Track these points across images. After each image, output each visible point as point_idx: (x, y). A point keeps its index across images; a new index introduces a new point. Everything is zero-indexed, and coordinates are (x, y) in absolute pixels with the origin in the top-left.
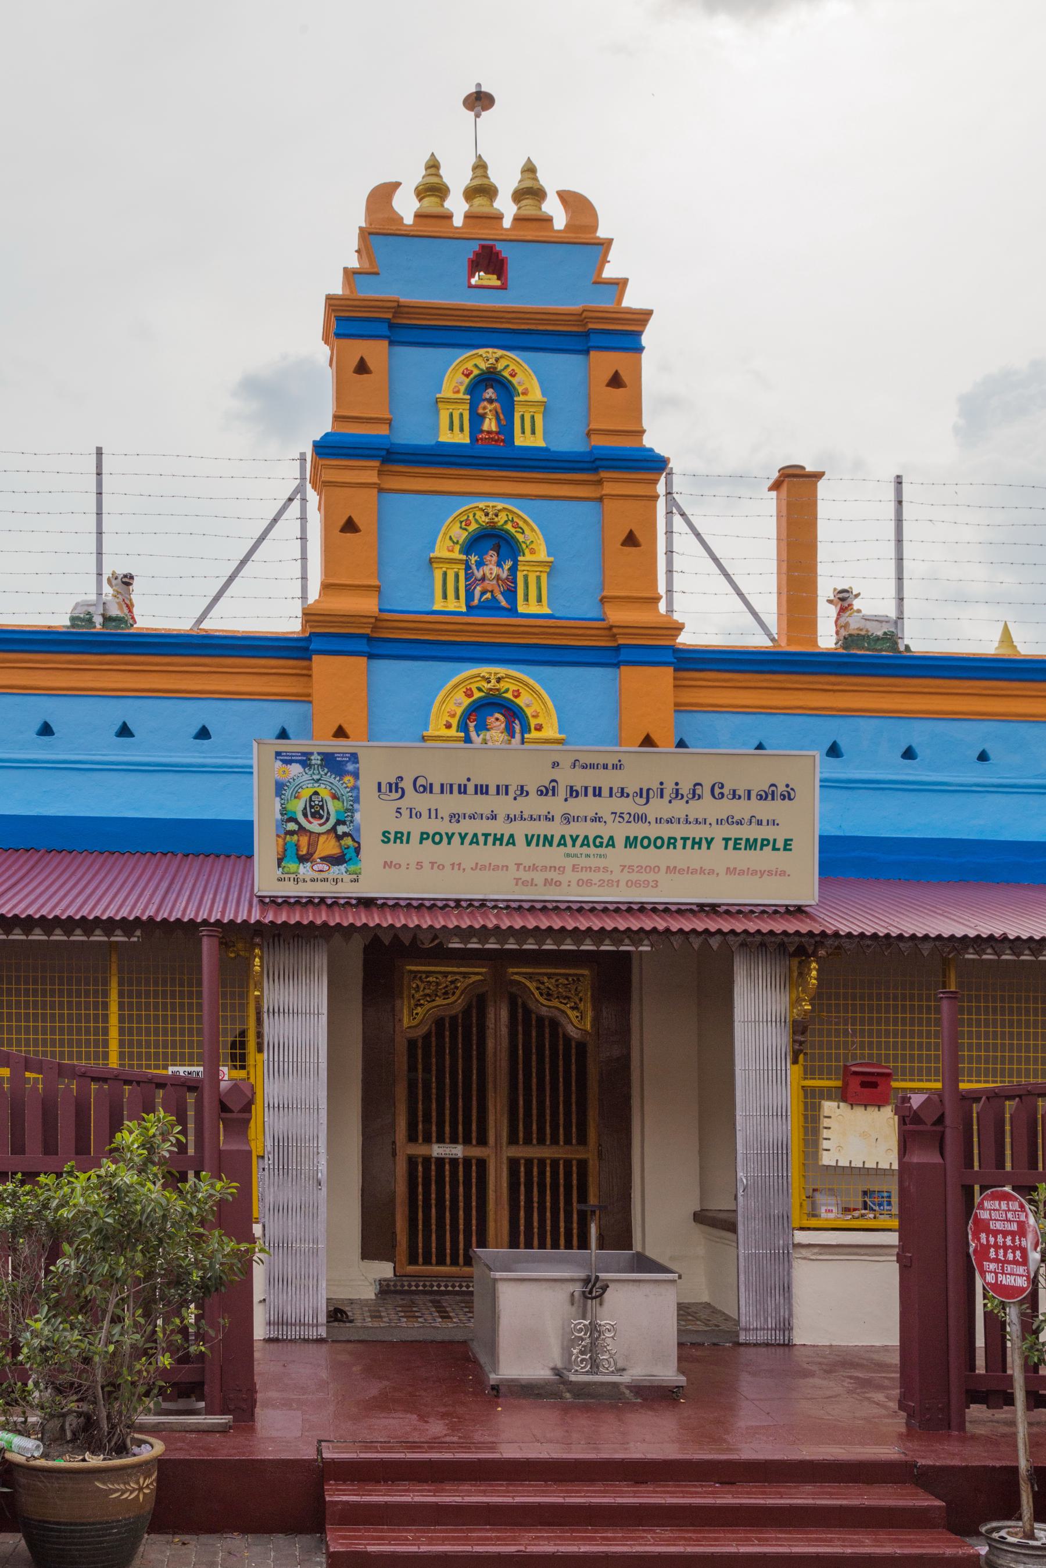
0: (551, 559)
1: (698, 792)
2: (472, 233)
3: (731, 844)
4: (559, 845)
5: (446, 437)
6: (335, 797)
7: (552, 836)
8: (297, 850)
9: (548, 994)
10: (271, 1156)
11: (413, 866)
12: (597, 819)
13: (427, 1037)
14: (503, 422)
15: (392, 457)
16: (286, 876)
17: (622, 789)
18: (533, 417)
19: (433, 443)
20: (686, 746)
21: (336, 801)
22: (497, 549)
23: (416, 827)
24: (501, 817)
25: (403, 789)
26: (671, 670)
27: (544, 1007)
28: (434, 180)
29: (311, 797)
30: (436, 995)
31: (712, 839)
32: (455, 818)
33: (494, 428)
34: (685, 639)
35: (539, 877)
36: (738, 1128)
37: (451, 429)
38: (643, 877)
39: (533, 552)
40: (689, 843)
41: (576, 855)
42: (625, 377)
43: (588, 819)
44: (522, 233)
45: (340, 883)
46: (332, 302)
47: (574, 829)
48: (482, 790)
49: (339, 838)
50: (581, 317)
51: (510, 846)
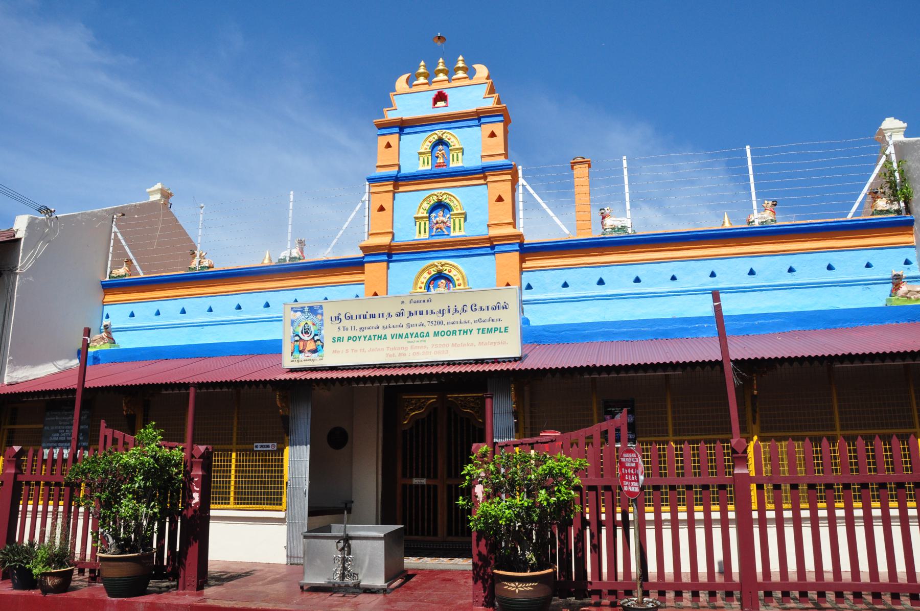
12: (421, 325)
32: (362, 329)
48: (373, 316)
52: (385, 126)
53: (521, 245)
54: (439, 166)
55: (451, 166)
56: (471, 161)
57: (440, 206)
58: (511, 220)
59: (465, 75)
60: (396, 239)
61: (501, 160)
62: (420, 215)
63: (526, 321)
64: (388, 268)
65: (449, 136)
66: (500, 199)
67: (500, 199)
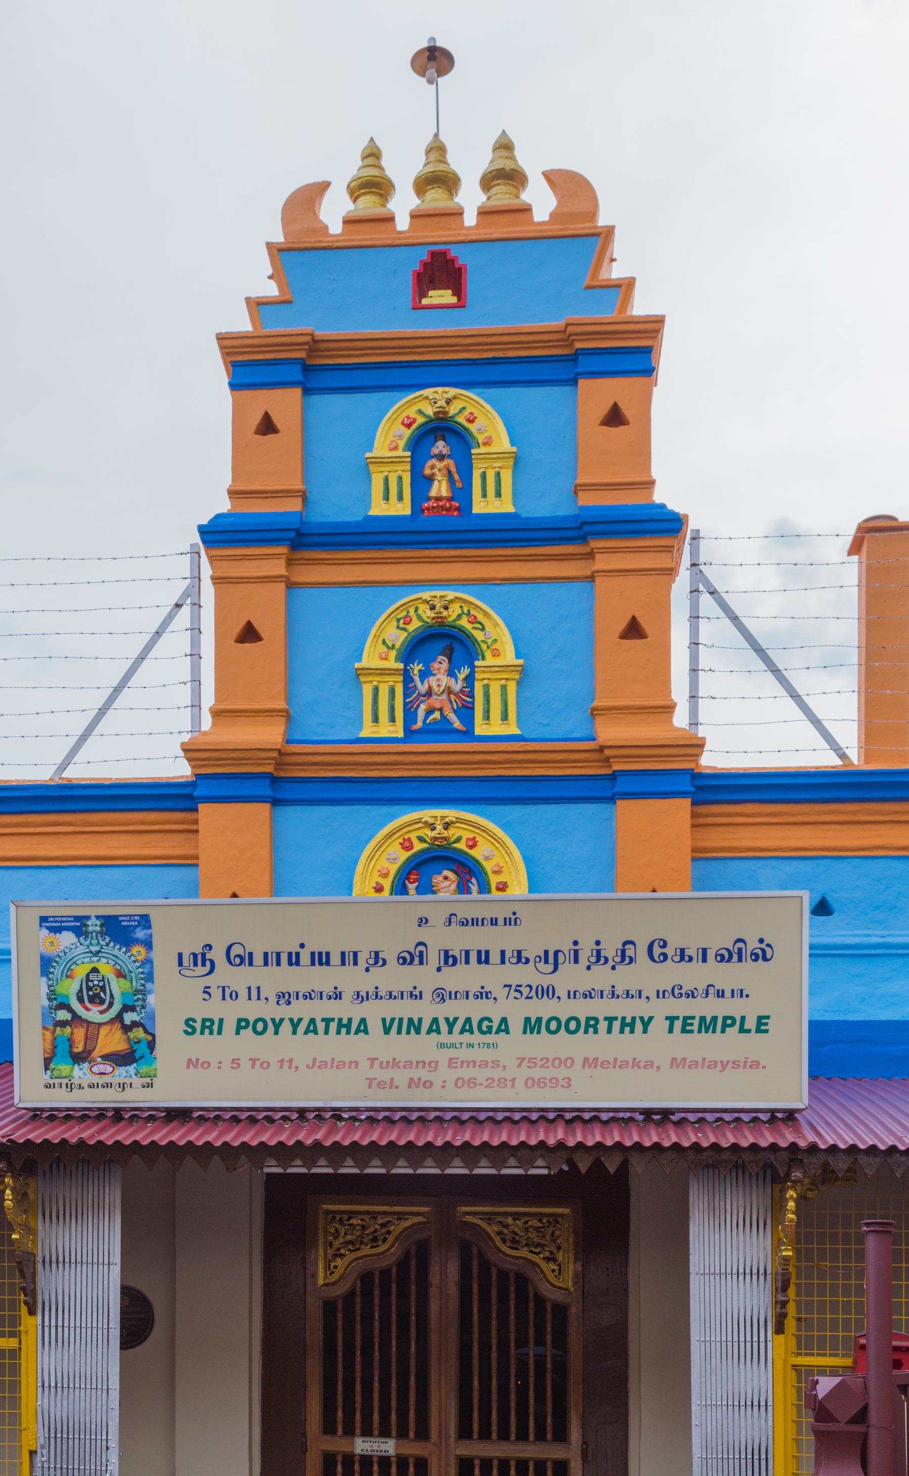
0: (521, 662)
1: (630, 952)
3: (678, 1024)
4: (429, 1032)
5: (379, 509)
6: (120, 974)
7: (420, 1020)
8: (71, 1047)
9: (514, 1241)
10: (44, 1452)
11: (227, 1064)
12: (483, 995)
13: (350, 1297)
14: (459, 485)
15: (303, 540)
16: (57, 1081)
17: (519, 952)
18: (498, 475)
19: (359, 518)
21: (121, 980)
22: (449, 653)
23: (230, 1012)
24: (348, 996)
25: (212, 962)
26: (687, 802)
27: (508, 1255)
28: (374, 172)
29: (88, 976)
30: (362, 1243)
32: (284, 998)
33: (445, 492)
34: (712, 760)
35: (401, 1077)
36: (694, 1422)
37: (386, 498)
38: (549, 1073)
39: (496, 654)
40: (616, 1025)
41: (453, 1046)
42: (627, 410)
43: (471, 995)
44: (488, 231)
45: (128, 1089)
46: (225, 343)
47: (451, 1009)
48: (321, 959)
49: (126, 1029)
50: (565, 335)
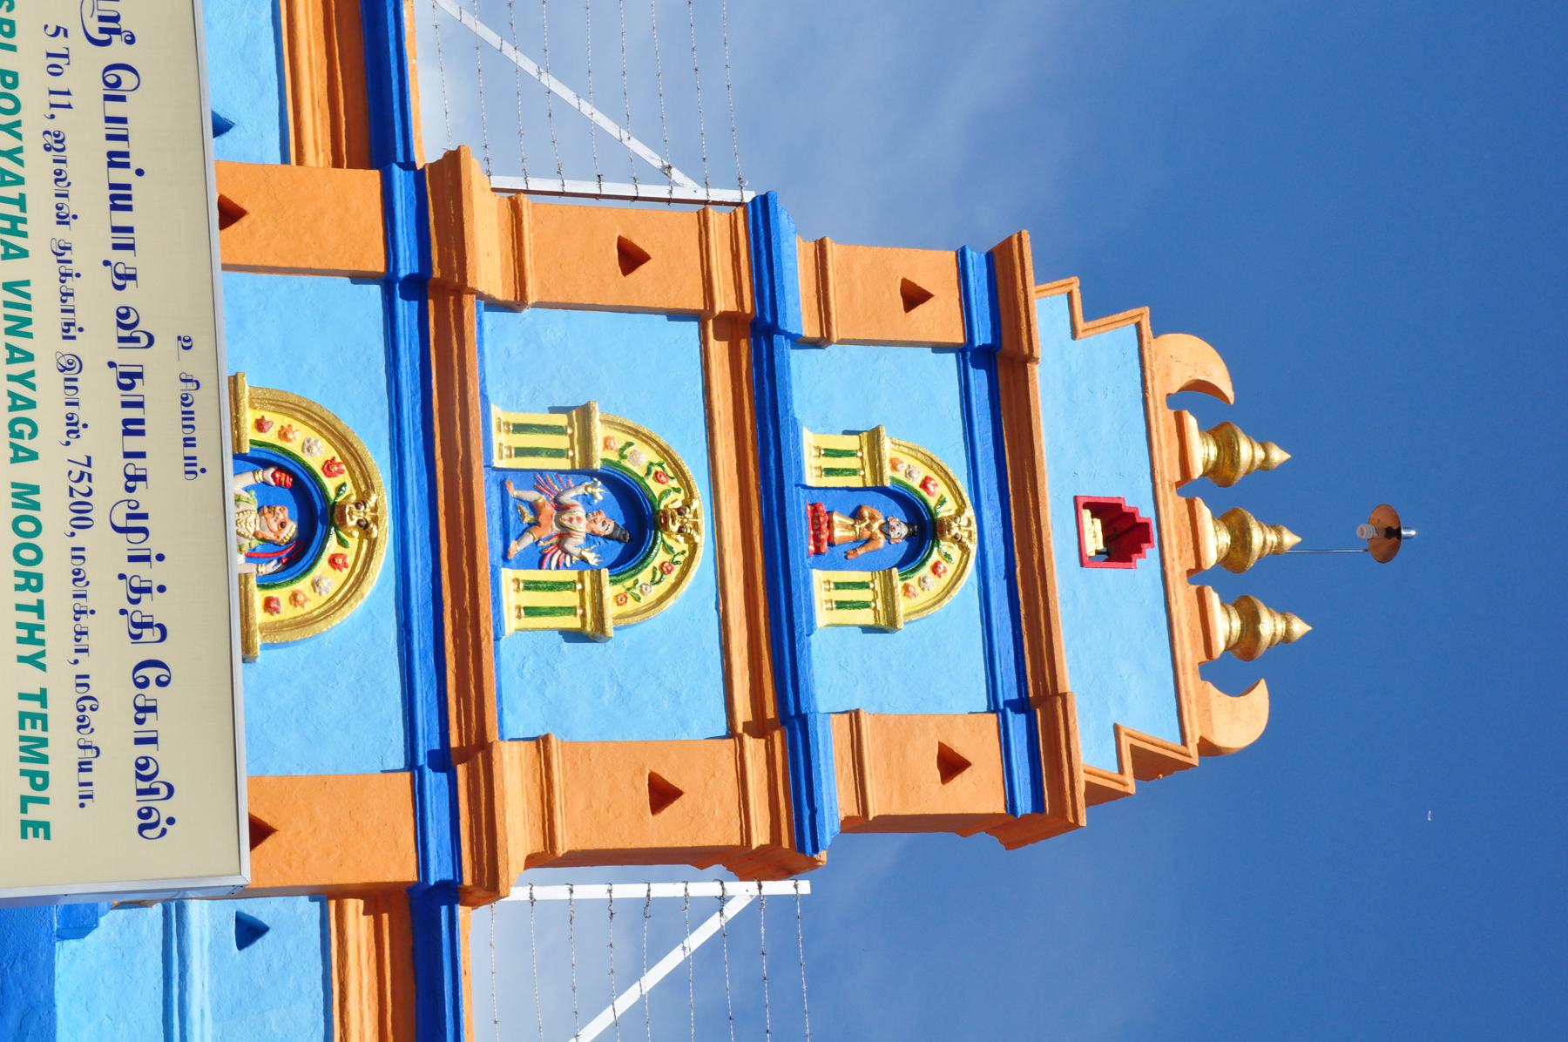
1: (147, 633)
2: (1166, 505)
3: (34, 707)
7: (29, 335)
12: (74, 427)
20: (224, 224)
31: (43, 667)
32: (56, 143)
48: (120, 198)
51: (11, 453)
52: (1000, 282)
53: (452, 892)
54: (819, 521)
55: (818, 576)
56: (837, 670)
57: (639, 525)
58: (563, 845)
59: (1220, 645)
60: (490, 318)
61: (836, 801)
62: (599, 431)
63: (78, 919)
64: (359, 278)
65: (950, 569)
66: (662, 794)
67: (662, 794)
